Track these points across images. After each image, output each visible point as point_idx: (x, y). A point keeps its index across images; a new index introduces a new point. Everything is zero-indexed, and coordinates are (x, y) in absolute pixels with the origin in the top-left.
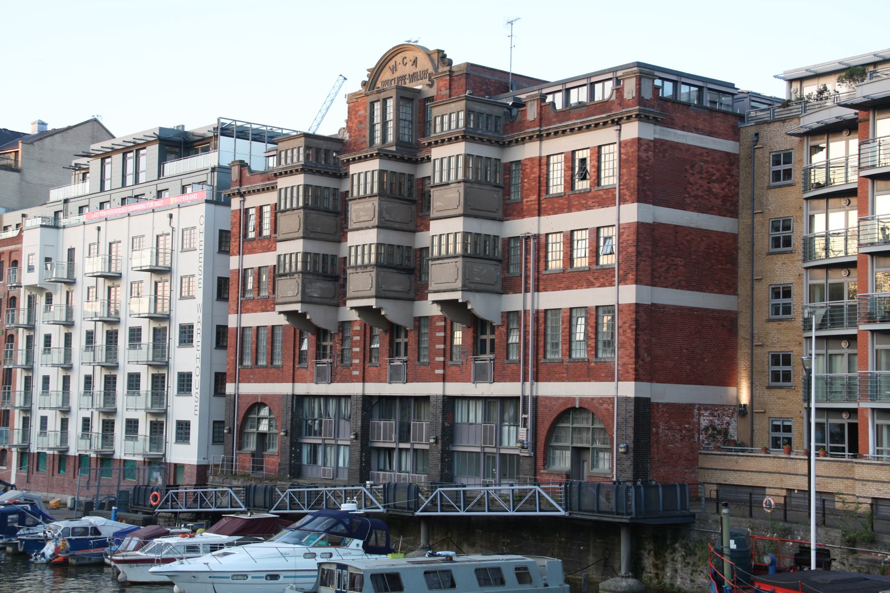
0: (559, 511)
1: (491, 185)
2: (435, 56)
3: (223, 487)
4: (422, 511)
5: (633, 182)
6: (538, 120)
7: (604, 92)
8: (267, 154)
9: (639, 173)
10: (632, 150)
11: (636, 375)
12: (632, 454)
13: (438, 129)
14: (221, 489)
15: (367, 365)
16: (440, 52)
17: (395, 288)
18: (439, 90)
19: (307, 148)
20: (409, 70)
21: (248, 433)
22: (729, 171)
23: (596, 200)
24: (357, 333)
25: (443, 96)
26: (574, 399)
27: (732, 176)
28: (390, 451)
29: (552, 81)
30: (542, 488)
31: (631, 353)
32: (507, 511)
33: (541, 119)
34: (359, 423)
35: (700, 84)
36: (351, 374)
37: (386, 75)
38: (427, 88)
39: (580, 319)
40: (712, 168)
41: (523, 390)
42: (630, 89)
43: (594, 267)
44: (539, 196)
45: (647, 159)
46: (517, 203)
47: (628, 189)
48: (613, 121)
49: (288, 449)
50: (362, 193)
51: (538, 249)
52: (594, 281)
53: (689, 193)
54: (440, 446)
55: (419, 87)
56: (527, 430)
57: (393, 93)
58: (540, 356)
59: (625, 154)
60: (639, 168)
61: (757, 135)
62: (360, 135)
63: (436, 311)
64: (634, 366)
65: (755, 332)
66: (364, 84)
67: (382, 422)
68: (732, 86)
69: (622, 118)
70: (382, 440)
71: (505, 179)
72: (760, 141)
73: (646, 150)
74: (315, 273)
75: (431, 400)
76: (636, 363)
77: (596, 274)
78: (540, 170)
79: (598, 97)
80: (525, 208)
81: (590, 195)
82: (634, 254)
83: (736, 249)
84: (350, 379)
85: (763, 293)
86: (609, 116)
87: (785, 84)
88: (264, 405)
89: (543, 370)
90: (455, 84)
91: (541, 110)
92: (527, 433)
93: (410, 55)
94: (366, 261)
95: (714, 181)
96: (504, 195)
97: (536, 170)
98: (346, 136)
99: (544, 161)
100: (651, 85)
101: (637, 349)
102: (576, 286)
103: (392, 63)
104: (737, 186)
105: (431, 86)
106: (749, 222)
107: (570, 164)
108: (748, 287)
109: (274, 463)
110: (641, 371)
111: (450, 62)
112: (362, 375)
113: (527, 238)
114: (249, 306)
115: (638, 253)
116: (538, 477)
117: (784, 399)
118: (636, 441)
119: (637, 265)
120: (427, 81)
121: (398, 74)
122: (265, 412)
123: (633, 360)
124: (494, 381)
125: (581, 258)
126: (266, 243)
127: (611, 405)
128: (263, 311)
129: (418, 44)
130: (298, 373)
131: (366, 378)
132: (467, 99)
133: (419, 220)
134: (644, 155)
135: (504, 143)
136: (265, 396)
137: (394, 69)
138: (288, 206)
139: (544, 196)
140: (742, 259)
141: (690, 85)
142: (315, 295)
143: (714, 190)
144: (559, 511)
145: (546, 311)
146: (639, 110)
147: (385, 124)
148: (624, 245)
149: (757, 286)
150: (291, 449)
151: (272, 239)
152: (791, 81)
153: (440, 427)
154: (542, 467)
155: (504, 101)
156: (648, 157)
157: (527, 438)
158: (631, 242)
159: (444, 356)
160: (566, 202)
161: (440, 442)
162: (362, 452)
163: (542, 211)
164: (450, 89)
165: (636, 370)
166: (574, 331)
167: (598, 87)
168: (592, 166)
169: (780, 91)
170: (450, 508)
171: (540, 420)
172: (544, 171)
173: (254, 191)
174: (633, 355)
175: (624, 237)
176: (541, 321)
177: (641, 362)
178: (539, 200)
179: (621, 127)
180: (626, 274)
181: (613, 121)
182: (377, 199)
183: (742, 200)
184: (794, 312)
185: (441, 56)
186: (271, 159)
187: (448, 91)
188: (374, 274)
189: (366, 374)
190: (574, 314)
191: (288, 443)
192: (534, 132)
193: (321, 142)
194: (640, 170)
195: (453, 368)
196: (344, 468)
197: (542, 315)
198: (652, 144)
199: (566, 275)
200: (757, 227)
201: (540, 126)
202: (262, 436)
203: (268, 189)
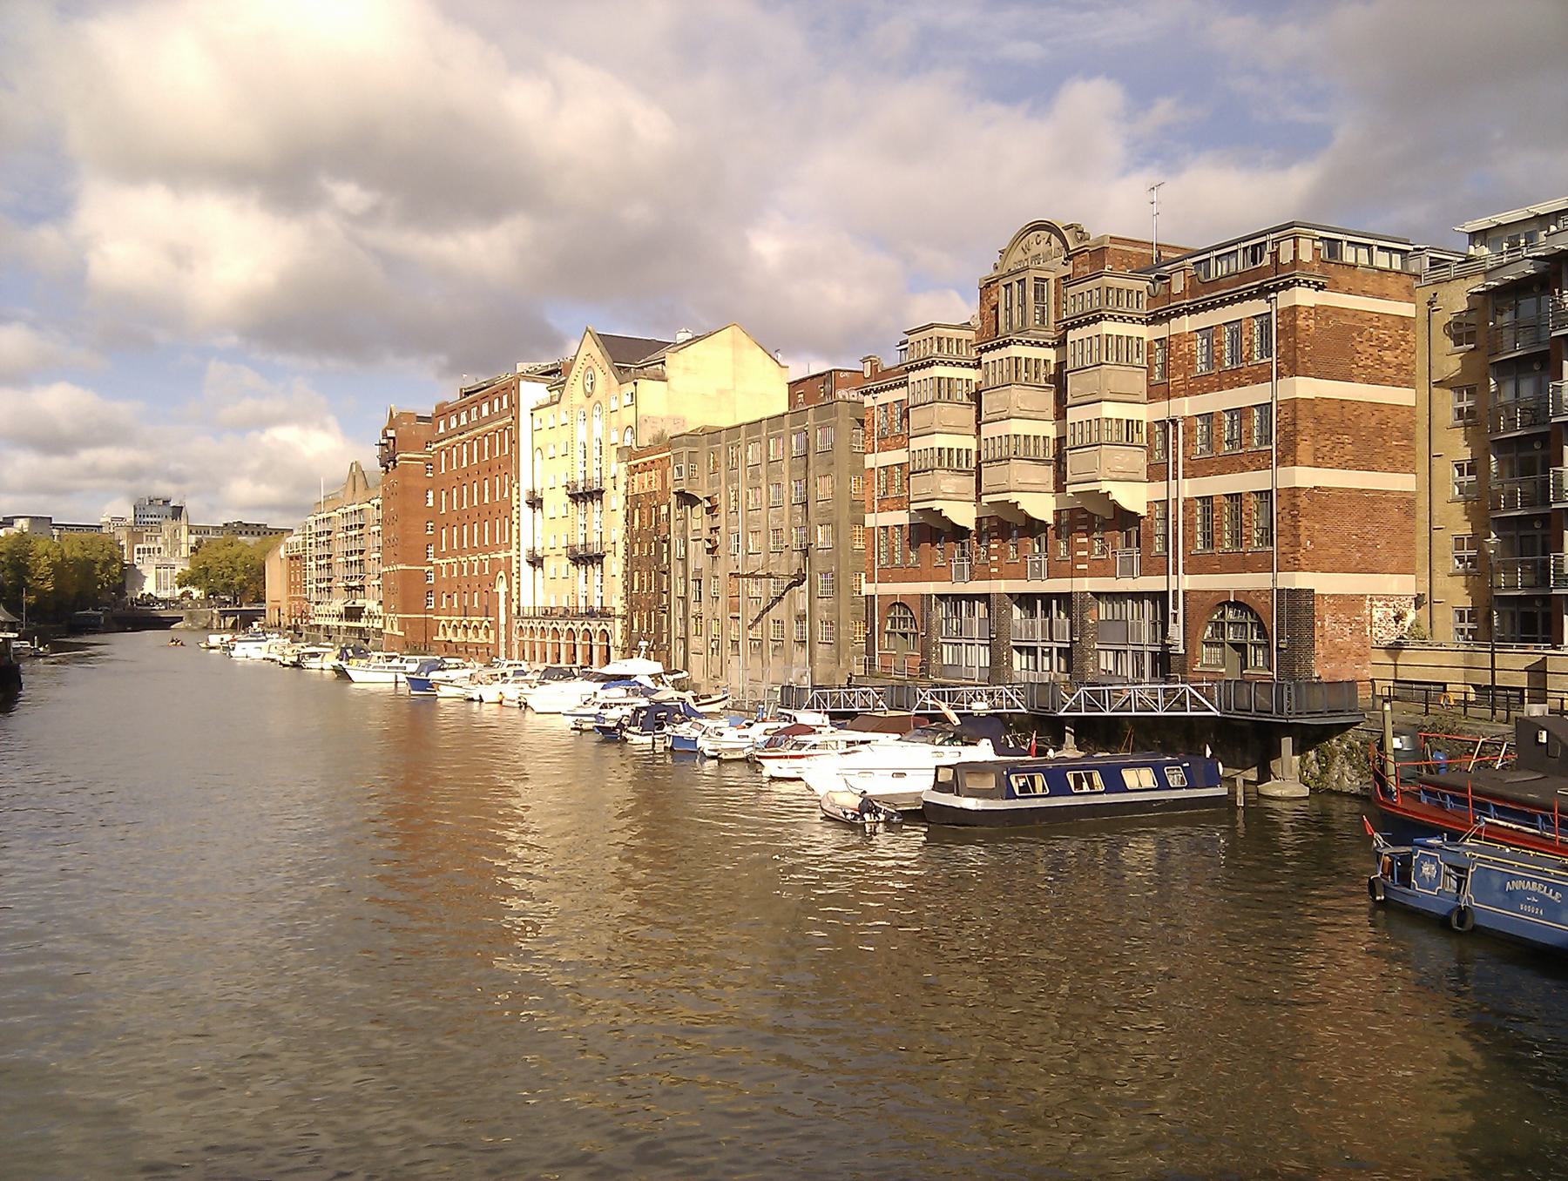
121: (1030, 254)
144: (1210, 710)
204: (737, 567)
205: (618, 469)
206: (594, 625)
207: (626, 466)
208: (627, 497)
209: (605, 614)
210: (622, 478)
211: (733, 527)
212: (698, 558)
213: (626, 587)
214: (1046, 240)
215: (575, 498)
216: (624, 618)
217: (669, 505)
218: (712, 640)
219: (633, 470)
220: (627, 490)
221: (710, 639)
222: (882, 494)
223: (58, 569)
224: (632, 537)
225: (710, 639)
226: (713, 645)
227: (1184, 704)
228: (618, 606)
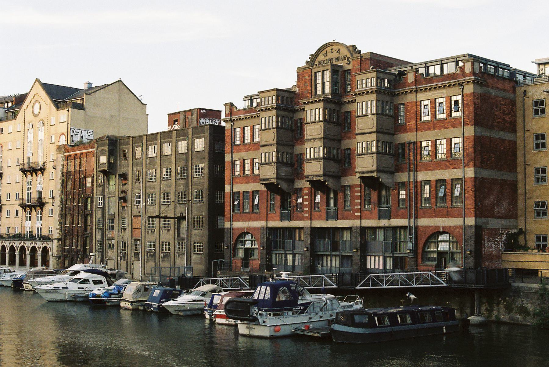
0: (443, 284)
1: (389, 116)
2: (351, 49)
3: (226, 277)
4: (359, 287)
5: (472, 115)
6: (414, 82)
7: (449, 69)
8: (245, 99)
9: (474, 110)
10: (470, 98)
11: (475, 214)
12: (473, 255)
13: (360, 86)
14: (226, 278)
15: (313, 211)
16: (354, 46)
17: (332, 170)
18: (354, 66)
19: (278, 96)
20: (335, 55)
21: (238, 248)
22: (512, 109)
23: (450, 124)
24: (306, 194)
25: (356, 70)
26: (439, 227)
27: (513, 112)
28: (323, 256)
29: (415, 63)
30: (325, 276)
31: (472, 203)
32: (382, 286)
33: (416, 82)
34: (309, 242)
35: (495, 65)
36: (303, 216)
37: (321, 57)
38: (346, 65)
39: (457, 185)
40: (505, 108)
41: (409, 222)
42: (468, 68)
43: (449, 158)
44: (416, 121)
45: (477, 103)
46: (403, 125)
47: (468, 118)
48: (459, 84)
49: (265, 257)
50: (313, 120)
51: (416, 149)
52: (450, 166)
53: (495, 121)
54: (359, 253)
55: (342, 64)
56: (412, 244)
57: (329, 67)
58: (418, 205)
59: (466, 101)
60: (474, 107)
61: (525, 91)
62: (305, 89)
63: (358, 182)
64: (474, 209)
65: (527, 191)
66: (307, 62)
67: (322, 241)
68: (508, 66)
69: (465, 82)
70: (322, 251)
71: (395, 113)
72: (528, 94)
73: (477, 99)
74: (283, 163)
75: (353, 229)
76: (475, 208)
77: (451, 162)
78: (416, 108)
79: (445, 72)
80: (408, 128)
81: (445, 121)
82: (473, 152)
83: (516, 149)
84: (303, 219)
85: (531, 171)
86: (457, 81)
87: (536, 66)
88: (248, 233)
89: (420, 212)
90: (364, 63)
91: (416, 78)
92: (412, 245)
93: (335, 48)
94: (317, 156)
95: (506, 114)
96: (395, 122)
97: (414, 108)
98: (297, 90)
99: (418, 103)
100: (478, 66)
101: (475, 201)
102: (438, 169)
103: (324, 52)
104: (516, 117)
105: (349, 64)
106: (523, 135)
107: (434, 105)
108: (523, 168)
109: (256, 264)
110: (478, 212)
111: (360, 52)
112: (310, 216)
113: (410, 144)
114: (237, 180)
115: (475, 151)
116: (418, 268)
117: (543, 225)
118: (476, 248)
119: (475, 157)
120: (346, 61)
121: (328, 58)
122: (248, 237)
123: (474, 206)
124: (291, 221)
125: (441, 154)
126: (248, 146)
127: (461, 230)
128: (246, 183)
129: (335, 41)
130: (269, 216)
131: (312, 218)
132: (377, 71)
133: (343, 134)
134: (476, 101)
135: (395, 94)
136: (249, 228)
137: (326, 55)
138: (267, 127)
139: (418, 122)
140: (520, 154)
141: (491, 65)
142: (283, 175)
143: (506, 119)
144: (443, 284)
145: (421, 181)
146: (475, 78)
147: (323, 84)
148: (467, 147)
149: (527, 167)
150: (266, 256)
151: (251, 144)
152: (539, 64)
153: (359, 243)
154: (421, 263)
155: (392, 72)
156: (478, 102)
157: (412, 248)
158: (471, 146)
159: (361, 206)
160: (432, 125)
161: (359, 251)
162: (311, 257)
163: (418, 129)
164: (361, 65)
165: (475, 211)
166: (423, 193)
167: (445, 66)
168: (447, 107)
169: (533, 70)
170: (377, 284)
171: (419, 238)
172: (419, 109)
173: (240, 119)
174: (473, 204)
175: (467, 143)
176: (419, 187)
177: (477, 208)
178: (416, 124)
179: (463, 87)
180: (469, 162)
181: (459, 84)
182: (323, 123)
183: (519, 123)
184: (548, 181)
185: (354, 48)
186: (247, 101)
187: (359, 67)
188: (322, 163)
189: (312, 215)
190: (454, 184)
191: (265, 253)
192: (413, 89)
193: (282, 92)
194: (475, 109)
195: (366, 212)
196: (298, 265)
197: (419, 184)
198: (480, 95)
199: (433, 163)
200: (527, 138)
201: (416, 86)
202: (247, 250)
203: (249, 118)
204: (139, 212)
205: (57, 158)
206: (39, 245)
207: (62, 155)
208: (62, 173)
209: (46, 238)
210: (60, 162)
211: (136, 191)
212: (114, 208)
213: (61, 223)
214: (337, 51)
215: (24, 171)
216: (59, 240)
217: (93, 177)
218: (121, 253)
219: (67, 158)
220: (63, 169)
221: (119, 251)
222: (239, 212)
223: (58, 265)
224: (66, 197)
225: (119, 251)
226: (121, 255)
227: (322, 283)
228: (56, 234)
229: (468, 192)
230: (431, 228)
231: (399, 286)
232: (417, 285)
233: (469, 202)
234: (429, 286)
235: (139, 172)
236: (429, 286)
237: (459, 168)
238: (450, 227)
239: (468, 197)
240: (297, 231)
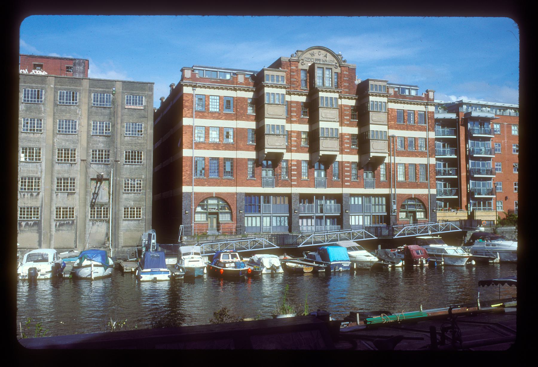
26: (412, 195)
175: (431, 142)
229: (432, 173)
230: (406, 195)
231: (364, 239)
232: (252, 249)
233: (433, 180)
234: (449, 231)
235: (73, 93)
236: (449, 231)
237: (425, 157)
238: (419, 195)
239: (432, 176)
240: (482, 133)
